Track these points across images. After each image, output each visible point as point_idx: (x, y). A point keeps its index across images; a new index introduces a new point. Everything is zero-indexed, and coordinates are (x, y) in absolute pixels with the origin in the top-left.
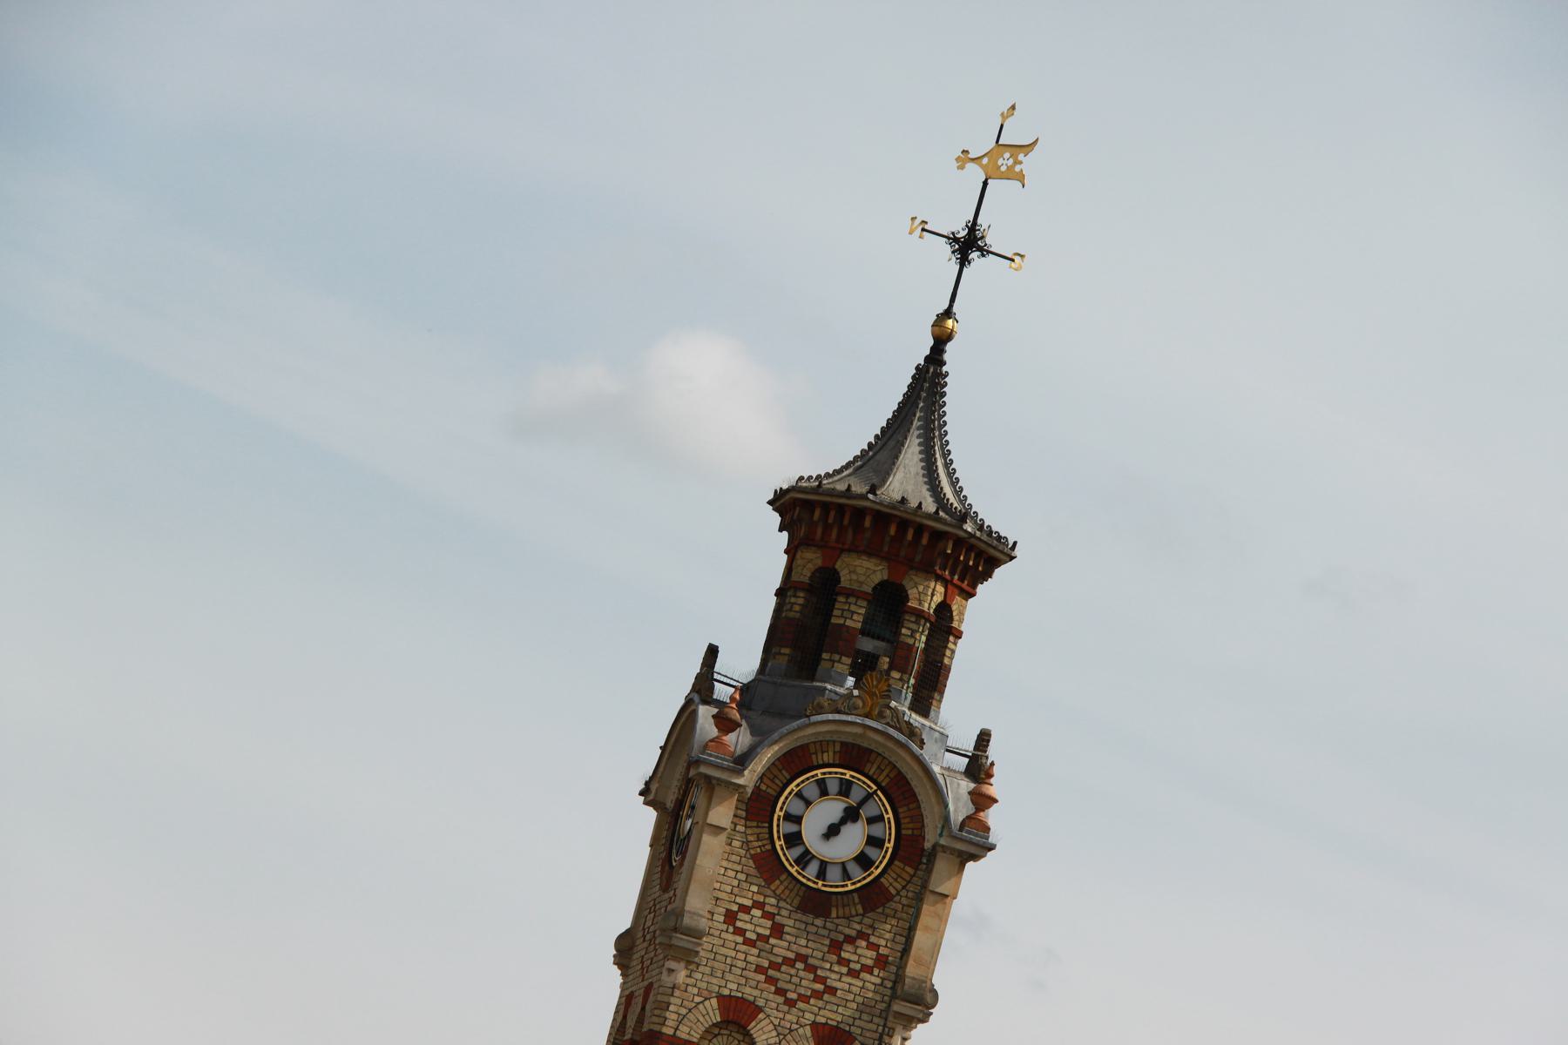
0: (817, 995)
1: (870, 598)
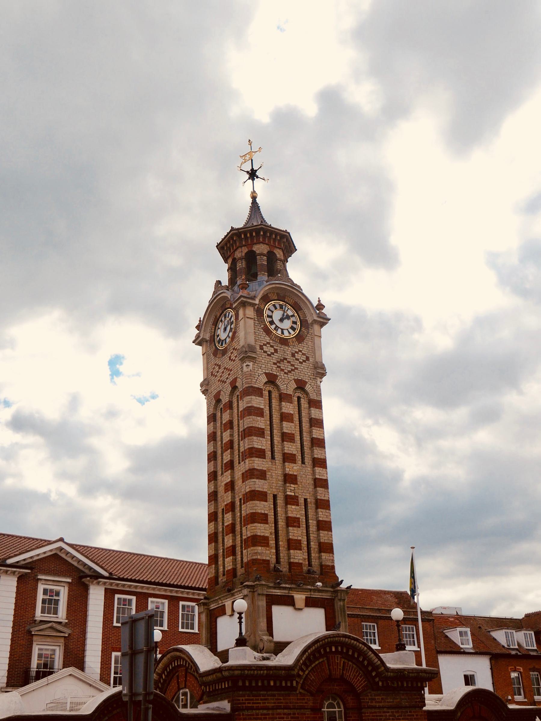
0: (292, 370)
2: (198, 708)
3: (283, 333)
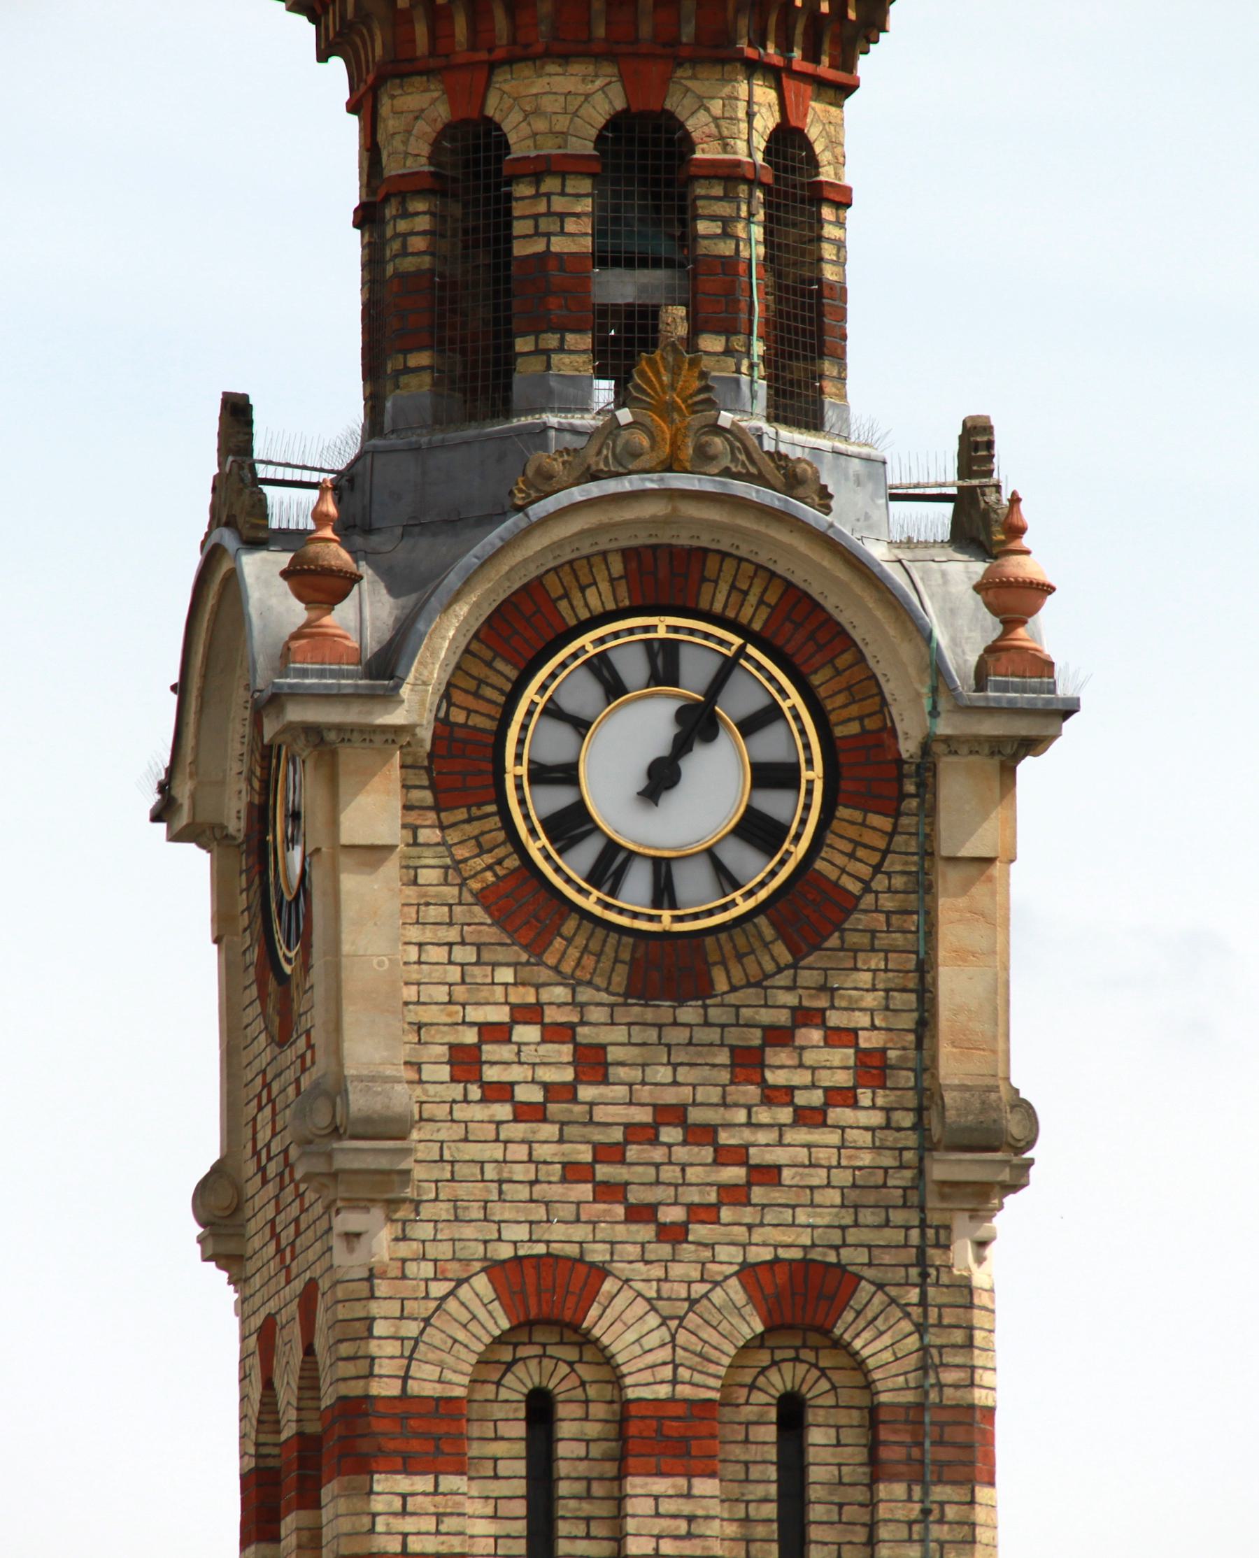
0: (734, 1195)
1: (597, 168)
2: (322, 57)
3: (664, 893)
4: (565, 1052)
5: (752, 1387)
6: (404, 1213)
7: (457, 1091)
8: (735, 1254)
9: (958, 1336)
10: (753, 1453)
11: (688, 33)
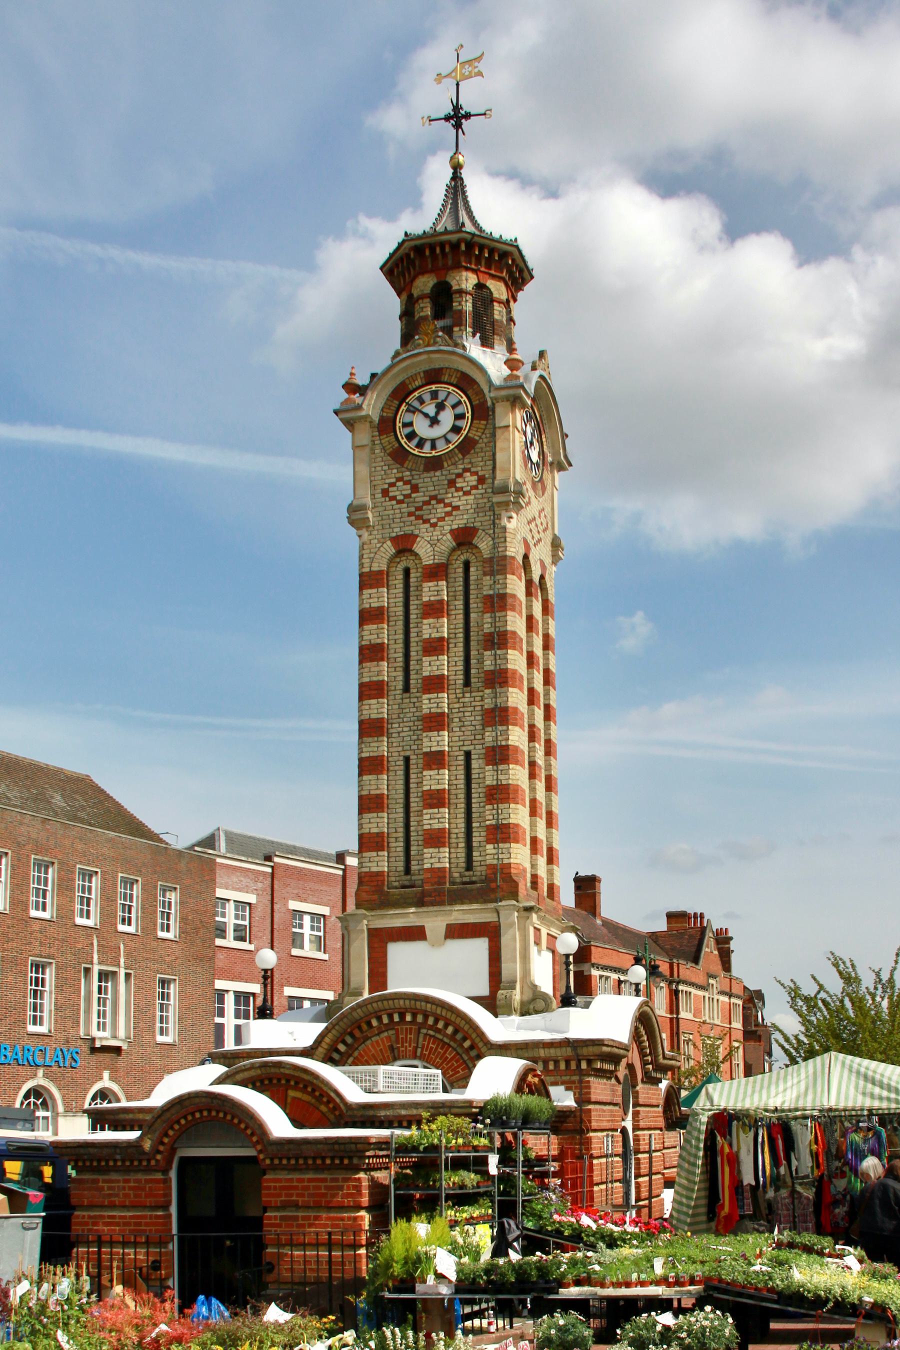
0: (448, 514)
3: (433, 447)
4: (409, 487)
5: (457, 560)
6: (371, 529)
7: (383, 499)
8: (449, 528)
9: (503, 540)
10: (457, 575)
11: (450, 262)
